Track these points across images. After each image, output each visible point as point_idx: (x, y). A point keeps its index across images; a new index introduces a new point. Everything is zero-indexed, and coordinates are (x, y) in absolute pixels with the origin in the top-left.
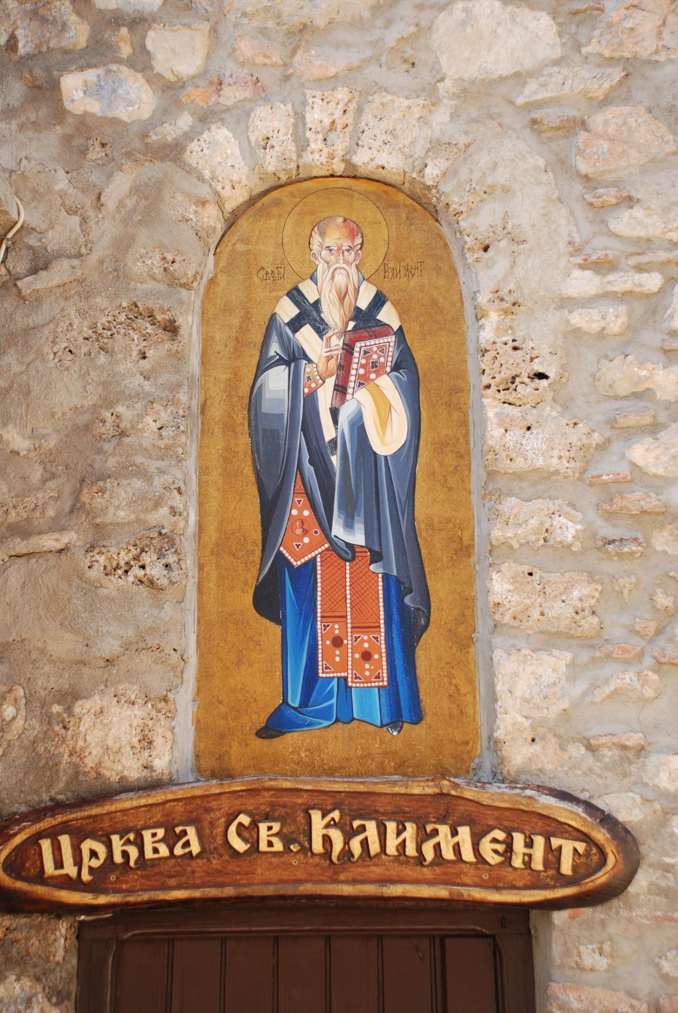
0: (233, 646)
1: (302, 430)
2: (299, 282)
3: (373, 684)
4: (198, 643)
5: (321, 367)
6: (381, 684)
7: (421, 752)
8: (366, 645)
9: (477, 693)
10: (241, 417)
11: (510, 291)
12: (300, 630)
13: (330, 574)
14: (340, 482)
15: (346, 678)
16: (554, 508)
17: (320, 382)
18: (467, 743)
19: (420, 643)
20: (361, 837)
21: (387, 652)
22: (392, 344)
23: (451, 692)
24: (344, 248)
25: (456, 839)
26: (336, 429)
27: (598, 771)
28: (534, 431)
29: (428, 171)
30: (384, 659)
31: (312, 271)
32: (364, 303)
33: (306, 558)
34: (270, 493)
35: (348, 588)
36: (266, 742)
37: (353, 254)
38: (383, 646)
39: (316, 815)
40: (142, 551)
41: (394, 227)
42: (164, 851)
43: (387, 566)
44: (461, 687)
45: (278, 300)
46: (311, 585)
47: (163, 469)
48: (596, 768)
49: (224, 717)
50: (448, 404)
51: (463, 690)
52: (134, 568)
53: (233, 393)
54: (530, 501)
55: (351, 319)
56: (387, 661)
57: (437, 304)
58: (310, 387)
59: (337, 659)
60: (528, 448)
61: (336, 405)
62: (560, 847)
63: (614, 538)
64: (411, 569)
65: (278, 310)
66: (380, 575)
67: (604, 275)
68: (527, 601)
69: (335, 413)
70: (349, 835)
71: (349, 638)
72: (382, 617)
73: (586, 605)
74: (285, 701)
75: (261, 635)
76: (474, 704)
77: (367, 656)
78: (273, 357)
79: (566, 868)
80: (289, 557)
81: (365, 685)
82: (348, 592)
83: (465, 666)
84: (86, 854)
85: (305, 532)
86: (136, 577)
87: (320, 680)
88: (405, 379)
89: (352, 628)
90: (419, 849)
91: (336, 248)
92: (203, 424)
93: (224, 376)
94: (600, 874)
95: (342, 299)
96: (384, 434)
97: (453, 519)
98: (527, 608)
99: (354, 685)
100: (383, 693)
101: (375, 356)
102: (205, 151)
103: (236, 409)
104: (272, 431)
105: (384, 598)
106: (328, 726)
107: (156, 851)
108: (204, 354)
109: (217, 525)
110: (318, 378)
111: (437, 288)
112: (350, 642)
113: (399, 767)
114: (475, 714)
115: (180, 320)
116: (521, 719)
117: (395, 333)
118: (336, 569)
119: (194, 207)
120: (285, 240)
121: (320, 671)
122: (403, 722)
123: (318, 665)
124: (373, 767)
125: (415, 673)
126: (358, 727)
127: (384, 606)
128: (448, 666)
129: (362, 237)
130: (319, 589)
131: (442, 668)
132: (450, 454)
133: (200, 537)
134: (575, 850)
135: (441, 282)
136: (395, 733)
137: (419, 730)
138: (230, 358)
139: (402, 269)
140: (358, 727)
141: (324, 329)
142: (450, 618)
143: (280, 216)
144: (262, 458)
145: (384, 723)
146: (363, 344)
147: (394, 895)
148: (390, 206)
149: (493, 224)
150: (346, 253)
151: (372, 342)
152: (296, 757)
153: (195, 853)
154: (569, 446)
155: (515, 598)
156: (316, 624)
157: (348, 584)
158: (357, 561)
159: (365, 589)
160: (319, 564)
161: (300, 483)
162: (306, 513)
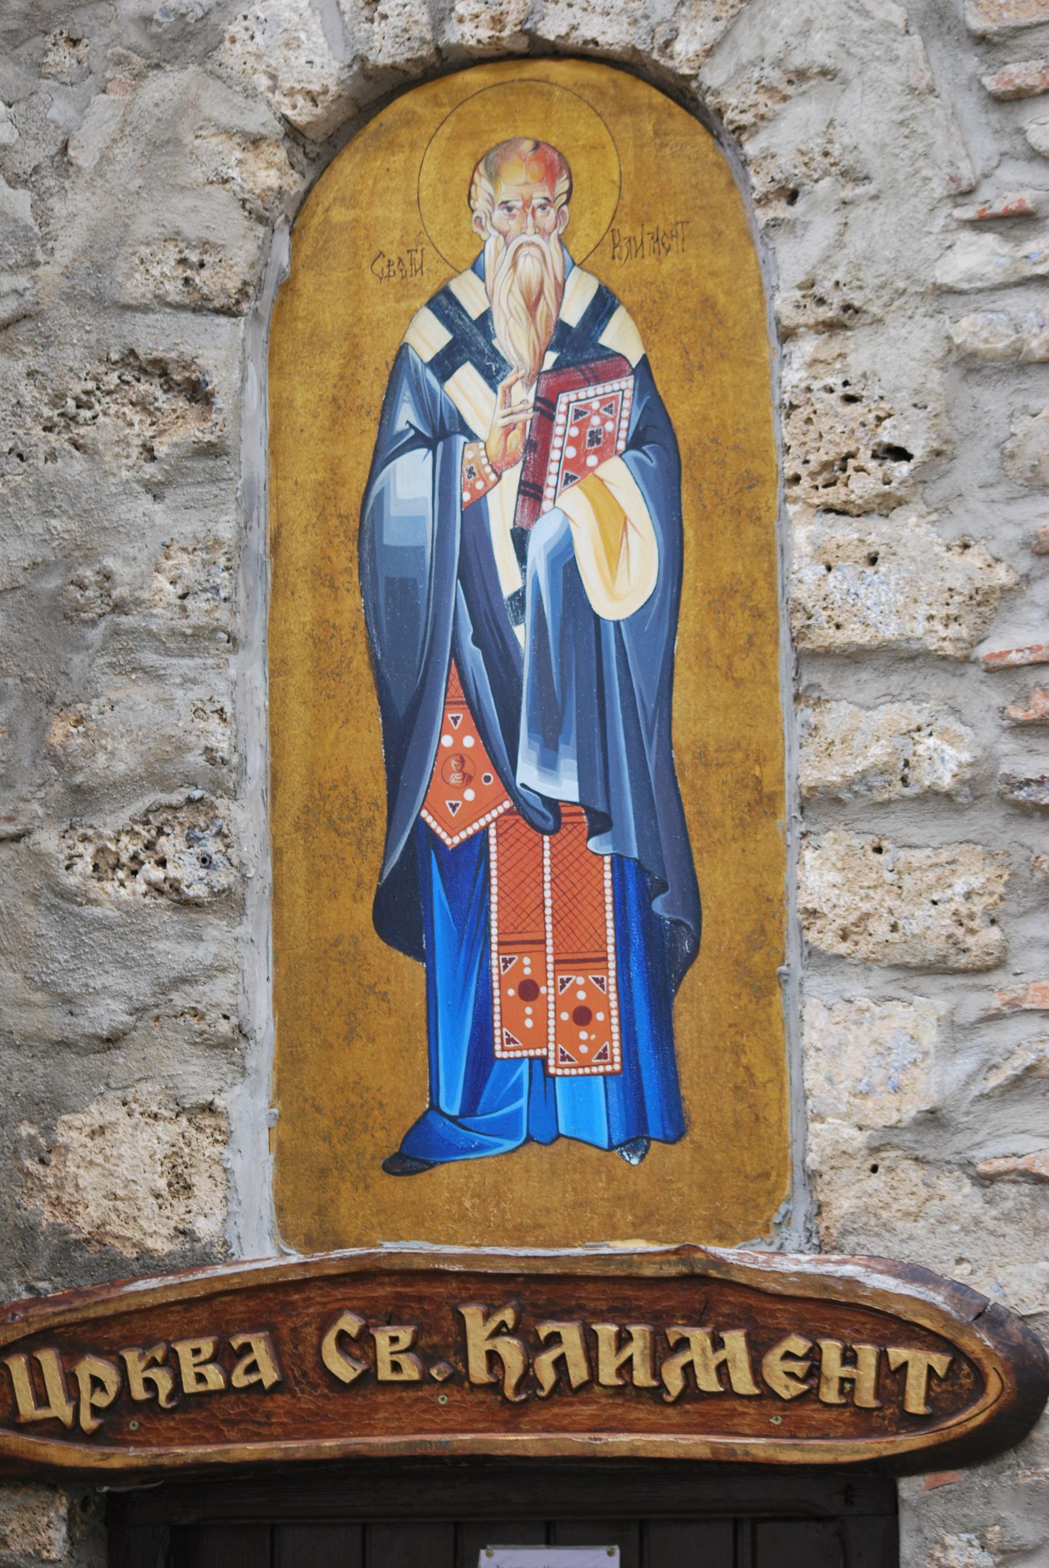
0: (339, 1003)
1: (459, 576)
2: (451, 278)
3: (594, 1070)
4: (277, 1000)
5: (495, 449)
6: (609, 1068)
7: (682, 1195)
8: (581, 995)
9: (787, 1080)
10: (344, 557)
11: (837, 283)
12: (461, 969)
13: (514, 860)
14: (532, 677)
15: (544, 1060)
16: (921, 720)
17: (493, 477)
18: (766, 1175)
19: (681, 989)
20: (554, 1353)
21: (619, 1008)
22: (628, 394)
23: (739, 1083)
24: (536, 202)
25: (722, 1355)
26: (524, 571)
27: (991, 1224)
28: (882, 567)
29: (679, 47)
30: (615, 1021)
31: (474, 253)
32: (573, 314)
33: (470, 831)
34: (401, 705)
35: (547, 886)
36: (403, 1181)
37: (553, 213)
38: (613, 996)
39: (472, 1314)
40: (160, 832)
41: (630, 153)
42: (215, 1378)
43: (619, 840)
44: (755, 1071)
45: (411, 315)
46: (479, 883)
47: (191, 675)
48: (986, 1219)
49: (327, 1138)
50: (736, 511)
51: (761, 1077)
52: (147, 866)
53: (330, 509)
54: (875, 707)
55: (551, 347)
56: (620, 1025)
57: (713, 307)
58: (472, 490)
59: (529, 1023)
60: (869, 603)
61: (523, 523)
62: (905, 1365)
63: (1029, 776)
64: (664, 844)
65: (413, 338)
66: (607, 859)
67: (1019, 242)
68: (866, 907)
69: (520, 539)
70: (534, 1347)
71: (550, 983)
72: (611, 940)
73: (978, 909)
74: (434, 1106)
75: (389, 981)
76: (781, 1103)
77: (582, 1016)
78: (403, 433)
79: (915, 1403)
80: (439, 830)
81: (581, 1071)
82: (547, 894)
83: (765, 1030)
84: (85, 1385)
85: (468, 780)
86: (149, 883)
87: (497, 1065)
88: (653, 464)
89: (556, 962)
90: (656, 1374)
91: (519, 204)
92: (275, 575)
93: (313, 476)
94: (973, 1410)
95: (532, 307)
96: (614, 577)
97: (744, 743)
98: (866, 916)
99: (559, 1072)
100: (612, 1085)
101: (596, 421)
102: (258, 38)
103: (336, 541)
104: (404, 582)
105: (614, 903)
106: (513, 1151)
107: (201, 1378)
108: (275, 434)
109: (304, 771)
110: (488, 469)
111: (713, 274)
112: (551, 991)
113: (642, 1224)
114: (781, 1119)
115: (216, 381)
116: (848, 1132)
117: (634, 372)
118: (525, 850)
119: (238, 154)
120: (423, 194)
121: (498, 1047)
122: (649, 1139)
123: (493, 1036)
124: (595, 1223)
125: (672, 1045)
126: (568, 1151)
127: (615, 919)
128: (732, 1031)
129: (570, 178)
130: (494, 890)
131: (722, 1036)
132: (739, 613)
133: (274, 797)
134: (931, 1369)
135: (722, 261)
136: (635, 1161)
137: (679, 1154)
138: (323, 440)
139: (647, 238)
140: (568, 1151)
141: (498, 371)
142: (738, 938)
143: (413, 145)
144: (385, 635)
145: (615, 1142)
146: (572, 396)
147: (616, 1454)
148: (622, 110)
149: (803, 148)
150: (539, 213)
151: (591, 391)
152: (455, 1208)
153: (267, 1383)
154: (947, 595)
155: (846, 899)
156: (489, 958)
157: (547, 878)
158: (564, 831)
159: (579, 886)
160: (493, 841)
161: (456, 682)
162: (469, 741)
